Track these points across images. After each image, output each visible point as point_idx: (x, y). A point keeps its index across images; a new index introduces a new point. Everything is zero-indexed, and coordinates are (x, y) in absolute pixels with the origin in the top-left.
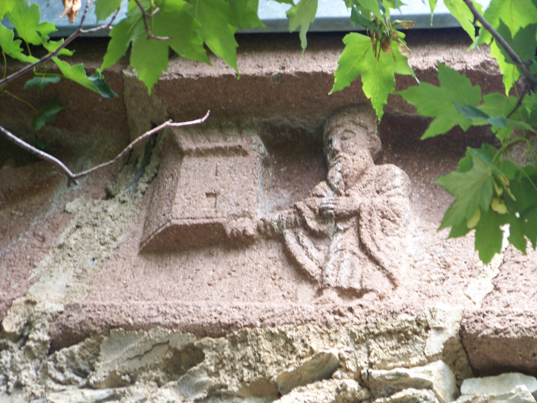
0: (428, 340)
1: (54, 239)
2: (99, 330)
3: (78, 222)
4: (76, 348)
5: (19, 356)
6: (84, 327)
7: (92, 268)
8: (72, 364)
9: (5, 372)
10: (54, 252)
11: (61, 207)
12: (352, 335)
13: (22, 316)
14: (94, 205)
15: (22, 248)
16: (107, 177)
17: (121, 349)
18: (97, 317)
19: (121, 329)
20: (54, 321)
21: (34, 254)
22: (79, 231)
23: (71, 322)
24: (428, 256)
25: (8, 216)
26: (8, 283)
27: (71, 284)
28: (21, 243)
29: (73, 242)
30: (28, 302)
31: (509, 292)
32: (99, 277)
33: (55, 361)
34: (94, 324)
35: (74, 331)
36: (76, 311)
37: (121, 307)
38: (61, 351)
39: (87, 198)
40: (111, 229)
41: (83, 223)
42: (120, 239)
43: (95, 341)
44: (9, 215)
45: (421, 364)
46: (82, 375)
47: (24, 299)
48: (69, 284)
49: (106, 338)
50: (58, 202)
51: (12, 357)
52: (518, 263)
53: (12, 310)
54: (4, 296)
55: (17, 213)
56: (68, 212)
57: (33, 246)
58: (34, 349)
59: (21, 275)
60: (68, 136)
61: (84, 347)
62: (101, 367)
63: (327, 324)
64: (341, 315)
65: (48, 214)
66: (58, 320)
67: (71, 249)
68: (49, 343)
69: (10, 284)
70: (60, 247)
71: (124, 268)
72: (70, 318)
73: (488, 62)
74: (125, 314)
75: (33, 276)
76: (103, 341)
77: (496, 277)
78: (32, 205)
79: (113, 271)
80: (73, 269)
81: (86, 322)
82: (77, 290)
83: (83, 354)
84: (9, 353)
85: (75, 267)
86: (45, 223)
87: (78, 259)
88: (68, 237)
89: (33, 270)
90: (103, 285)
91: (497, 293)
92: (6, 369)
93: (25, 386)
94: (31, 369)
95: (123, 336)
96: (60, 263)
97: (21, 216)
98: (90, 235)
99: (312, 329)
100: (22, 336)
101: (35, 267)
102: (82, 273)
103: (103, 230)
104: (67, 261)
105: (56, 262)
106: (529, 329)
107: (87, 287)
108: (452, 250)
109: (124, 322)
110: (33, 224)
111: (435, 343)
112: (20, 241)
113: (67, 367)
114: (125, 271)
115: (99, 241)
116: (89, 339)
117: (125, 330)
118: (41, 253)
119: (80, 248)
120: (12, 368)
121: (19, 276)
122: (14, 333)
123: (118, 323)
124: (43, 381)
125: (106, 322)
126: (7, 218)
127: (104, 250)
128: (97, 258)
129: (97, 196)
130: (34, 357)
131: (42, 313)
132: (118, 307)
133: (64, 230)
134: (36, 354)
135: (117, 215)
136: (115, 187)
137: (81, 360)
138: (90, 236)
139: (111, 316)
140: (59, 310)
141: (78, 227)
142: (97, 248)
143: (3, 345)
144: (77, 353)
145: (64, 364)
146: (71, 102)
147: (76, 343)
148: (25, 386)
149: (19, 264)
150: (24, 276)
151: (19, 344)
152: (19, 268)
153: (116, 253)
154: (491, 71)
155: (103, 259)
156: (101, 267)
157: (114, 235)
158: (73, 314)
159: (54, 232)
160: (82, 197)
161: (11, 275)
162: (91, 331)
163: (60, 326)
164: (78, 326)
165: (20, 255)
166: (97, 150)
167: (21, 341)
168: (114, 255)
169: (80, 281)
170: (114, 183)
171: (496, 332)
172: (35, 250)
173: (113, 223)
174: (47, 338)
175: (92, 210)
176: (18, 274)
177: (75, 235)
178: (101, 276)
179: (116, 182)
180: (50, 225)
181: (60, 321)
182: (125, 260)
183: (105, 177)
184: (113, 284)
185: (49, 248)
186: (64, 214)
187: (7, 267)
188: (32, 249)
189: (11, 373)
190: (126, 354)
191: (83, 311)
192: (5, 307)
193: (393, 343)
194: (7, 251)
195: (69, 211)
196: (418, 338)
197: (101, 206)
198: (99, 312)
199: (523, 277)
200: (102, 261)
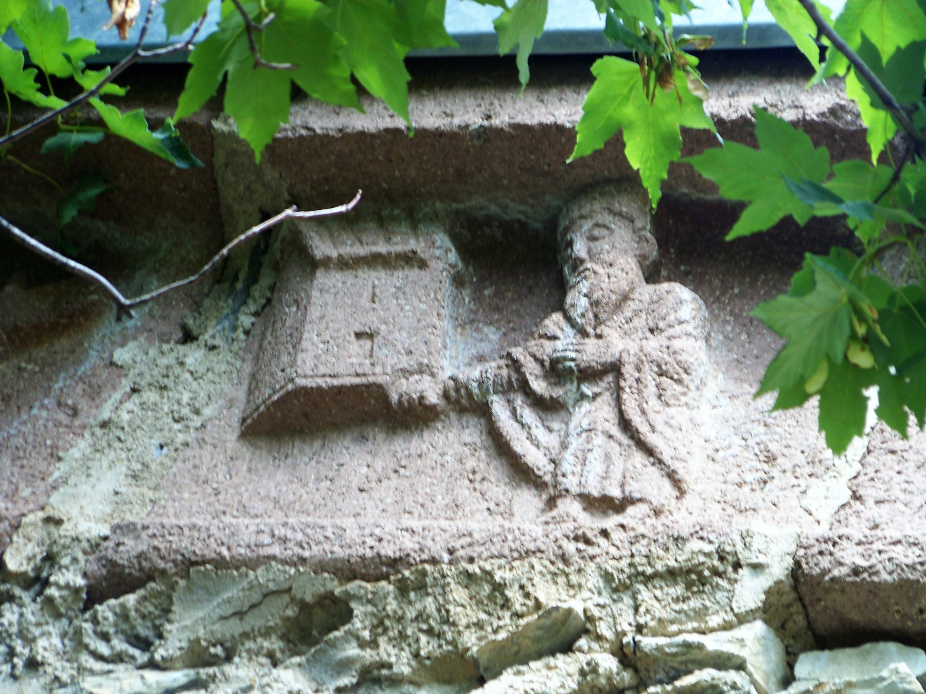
0: (737, 586)
1: (94, 411)
2: (171, 568)
3: (134, 383)
4: (131, 599)
5: (33, 613)
6: (144, 564)
7: (158, 461)
8: (125, 626)
9: (8, 641)
10: (93, 434)
11: (105, 356)
12: (607, 577)
13: (38, 545)
14: (162, 353)
15: (37, 427)
16: (185, 305)
17: (208, 601)
18: (168, 545)
19: (208, 566)
20: (94, 552)
21: (58, 437)
22: (135, 397)
23: (123, 555)
24: (737, 441)
25: (13, 373)
26: (13, 487)
27: (123, 490)
28: (36, 418)
29: (126, 417)
30: (48, 520)
31: (878, 502)
32: (171, 477)
33: (95, 621)
34: (163, 558)
35: (127, 571)
36: (131, 536)
37: (208, 529)
38: (105, 604)
39: (150, 341)
40: (191, 395)
41: (143, 383)
42: (207, 412)
43: (164, 588)
44: (16, 371)
45: (727, 627)
46: (142, 645)
47: (41, 515)
48: (118, 489)
49: (182, 583)
50: (99, 348)
51: (21, 615)
52: (893, 452)
53: (20, 535)
54: (7, 509)
55: (30, 367)
56: (117, 366)
57: (58, 424)
58: (58, 601)
59: (37, 473)
60: (117, 235)
61: (145, 598)
62: (175, 631)
63: (564, 559)
64: (588, 542)
65: (83, 369)
66: (100, 551)
67: (123, 428)
68: (85, 590)
69: (17, 489)
70: (104, 425)
71: (214, 462)
72: (121, 548)
73: (842, 107)
74: (216, 540)
75: (56, 474)
76: (177, 588)
77: (855, 477)
78: (55, 352)
79: (195, 467)
80: (126, 463)
81: (148, 555)
82: (134, 499)
83: (142, 609)
84: (15, 608)
85: (129, 460)
86: (77, 383)
87: (134, 446)
88: (117, 408)
89: (57, 465)
90: (178, 492)
91: (857, 505)
92: (10, 636)
93: (43, 664)
94: (54, 635)
95: (212, 579)
96: (103, 453)
97: (36, 373)
98: (156, 405)
99: (538, 567)
100: (37, 579)
101: (60, 459)
102: (142, 471)
103: (177, 396)
104: (115, 450)
105: (97, 451)
106: (912, 567)
107: (151, 494)
108: (779, 430)
109: (213, 555)
110: (56, 386)
111: (750, 591)
112: (35, 416)
113: (116, 632)
114: (215, 466)
115: (170, 416)
116: (153, 585)
117: (216, 568)
118: (71, 435)
119: (138, 427)
120: (21, 634)
121: (33, 476)
122: (25, 573)
123: (203, 556)
124: (74, 656)
125: (183, 555)
126: (12, 376)
127: (179, 431)
128: (167, 445)
129: (167, 337)
130: (58, 616)
131: (73, 539)
132: (203, 529)
133: (110, 396)
134: (62, 610)
135: (202, 370)
136: (198, 322)
137: (140, 621)
138: (155, 407)
139: (192, 544)
140: (102, 534)
141: (134, 390)
142: (166, 428)
143: (5, 595)
144: (133, 608)
145: (110, 626)
146: (123, 175)
147: (132, 590)
148: (43, 664)
149: (33, 455)
150: (41, 476)
151: (32, 592)
152: (33, 462)
153: (200, 436)
154: (847, 123)
155: (178, 445)
156: (175, 460)
157: (197, 405)
158: (126, 541)
159: (93, 399)
160: (142, 340)
161: (19, 474)
162: (156, 569)
163: (104, 562)
164: (135, 561)
165: (35, 440)
166: (168, 257)
167: (37, 587)
168: (197, 440)
169: (139, 483)
170: (196, 315)
171: (856, 571)
172: (61, 430)
173: (195, 384)
174: (80, 582)
175: (158, 362)
176: (31, 472)
177: (129, 405)
178: (175, 475)
179: (200, 314)
180: (86, 387)
181: (104, 553)
182: (215, 447)
183: (182, 305)
184: (194, 489)
185: (84, 427)
186: (110, 369)
187: (13, 460)
188: (55, 429)
189: (19, 642)
190: (217, 610)
191: (144, 535)
192: (8, 529)
193: (679, 590)
194: (12, 432)
195: (119, 363)
196: (720, 581)
197: (175, 354)
198: (171, 538)
199: (902, 478)
200: (176, 450)
